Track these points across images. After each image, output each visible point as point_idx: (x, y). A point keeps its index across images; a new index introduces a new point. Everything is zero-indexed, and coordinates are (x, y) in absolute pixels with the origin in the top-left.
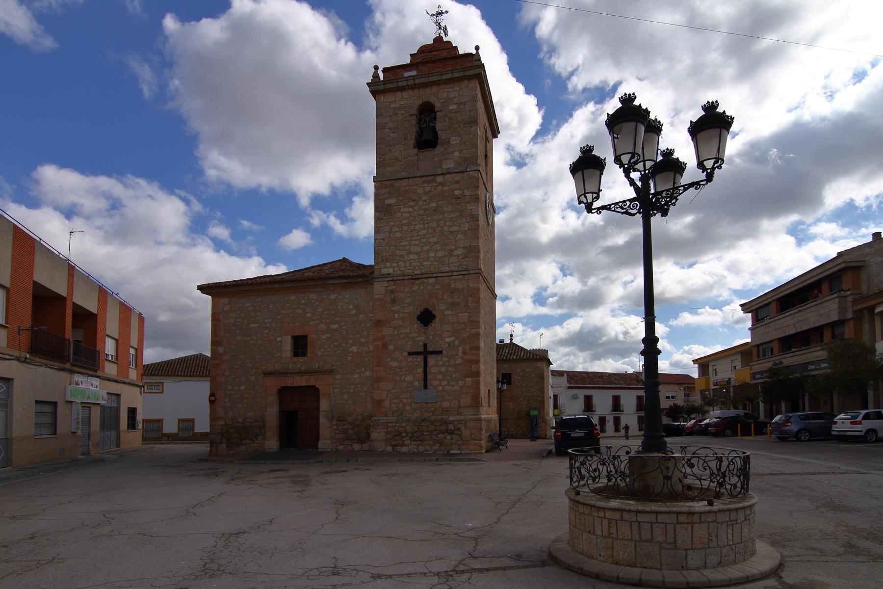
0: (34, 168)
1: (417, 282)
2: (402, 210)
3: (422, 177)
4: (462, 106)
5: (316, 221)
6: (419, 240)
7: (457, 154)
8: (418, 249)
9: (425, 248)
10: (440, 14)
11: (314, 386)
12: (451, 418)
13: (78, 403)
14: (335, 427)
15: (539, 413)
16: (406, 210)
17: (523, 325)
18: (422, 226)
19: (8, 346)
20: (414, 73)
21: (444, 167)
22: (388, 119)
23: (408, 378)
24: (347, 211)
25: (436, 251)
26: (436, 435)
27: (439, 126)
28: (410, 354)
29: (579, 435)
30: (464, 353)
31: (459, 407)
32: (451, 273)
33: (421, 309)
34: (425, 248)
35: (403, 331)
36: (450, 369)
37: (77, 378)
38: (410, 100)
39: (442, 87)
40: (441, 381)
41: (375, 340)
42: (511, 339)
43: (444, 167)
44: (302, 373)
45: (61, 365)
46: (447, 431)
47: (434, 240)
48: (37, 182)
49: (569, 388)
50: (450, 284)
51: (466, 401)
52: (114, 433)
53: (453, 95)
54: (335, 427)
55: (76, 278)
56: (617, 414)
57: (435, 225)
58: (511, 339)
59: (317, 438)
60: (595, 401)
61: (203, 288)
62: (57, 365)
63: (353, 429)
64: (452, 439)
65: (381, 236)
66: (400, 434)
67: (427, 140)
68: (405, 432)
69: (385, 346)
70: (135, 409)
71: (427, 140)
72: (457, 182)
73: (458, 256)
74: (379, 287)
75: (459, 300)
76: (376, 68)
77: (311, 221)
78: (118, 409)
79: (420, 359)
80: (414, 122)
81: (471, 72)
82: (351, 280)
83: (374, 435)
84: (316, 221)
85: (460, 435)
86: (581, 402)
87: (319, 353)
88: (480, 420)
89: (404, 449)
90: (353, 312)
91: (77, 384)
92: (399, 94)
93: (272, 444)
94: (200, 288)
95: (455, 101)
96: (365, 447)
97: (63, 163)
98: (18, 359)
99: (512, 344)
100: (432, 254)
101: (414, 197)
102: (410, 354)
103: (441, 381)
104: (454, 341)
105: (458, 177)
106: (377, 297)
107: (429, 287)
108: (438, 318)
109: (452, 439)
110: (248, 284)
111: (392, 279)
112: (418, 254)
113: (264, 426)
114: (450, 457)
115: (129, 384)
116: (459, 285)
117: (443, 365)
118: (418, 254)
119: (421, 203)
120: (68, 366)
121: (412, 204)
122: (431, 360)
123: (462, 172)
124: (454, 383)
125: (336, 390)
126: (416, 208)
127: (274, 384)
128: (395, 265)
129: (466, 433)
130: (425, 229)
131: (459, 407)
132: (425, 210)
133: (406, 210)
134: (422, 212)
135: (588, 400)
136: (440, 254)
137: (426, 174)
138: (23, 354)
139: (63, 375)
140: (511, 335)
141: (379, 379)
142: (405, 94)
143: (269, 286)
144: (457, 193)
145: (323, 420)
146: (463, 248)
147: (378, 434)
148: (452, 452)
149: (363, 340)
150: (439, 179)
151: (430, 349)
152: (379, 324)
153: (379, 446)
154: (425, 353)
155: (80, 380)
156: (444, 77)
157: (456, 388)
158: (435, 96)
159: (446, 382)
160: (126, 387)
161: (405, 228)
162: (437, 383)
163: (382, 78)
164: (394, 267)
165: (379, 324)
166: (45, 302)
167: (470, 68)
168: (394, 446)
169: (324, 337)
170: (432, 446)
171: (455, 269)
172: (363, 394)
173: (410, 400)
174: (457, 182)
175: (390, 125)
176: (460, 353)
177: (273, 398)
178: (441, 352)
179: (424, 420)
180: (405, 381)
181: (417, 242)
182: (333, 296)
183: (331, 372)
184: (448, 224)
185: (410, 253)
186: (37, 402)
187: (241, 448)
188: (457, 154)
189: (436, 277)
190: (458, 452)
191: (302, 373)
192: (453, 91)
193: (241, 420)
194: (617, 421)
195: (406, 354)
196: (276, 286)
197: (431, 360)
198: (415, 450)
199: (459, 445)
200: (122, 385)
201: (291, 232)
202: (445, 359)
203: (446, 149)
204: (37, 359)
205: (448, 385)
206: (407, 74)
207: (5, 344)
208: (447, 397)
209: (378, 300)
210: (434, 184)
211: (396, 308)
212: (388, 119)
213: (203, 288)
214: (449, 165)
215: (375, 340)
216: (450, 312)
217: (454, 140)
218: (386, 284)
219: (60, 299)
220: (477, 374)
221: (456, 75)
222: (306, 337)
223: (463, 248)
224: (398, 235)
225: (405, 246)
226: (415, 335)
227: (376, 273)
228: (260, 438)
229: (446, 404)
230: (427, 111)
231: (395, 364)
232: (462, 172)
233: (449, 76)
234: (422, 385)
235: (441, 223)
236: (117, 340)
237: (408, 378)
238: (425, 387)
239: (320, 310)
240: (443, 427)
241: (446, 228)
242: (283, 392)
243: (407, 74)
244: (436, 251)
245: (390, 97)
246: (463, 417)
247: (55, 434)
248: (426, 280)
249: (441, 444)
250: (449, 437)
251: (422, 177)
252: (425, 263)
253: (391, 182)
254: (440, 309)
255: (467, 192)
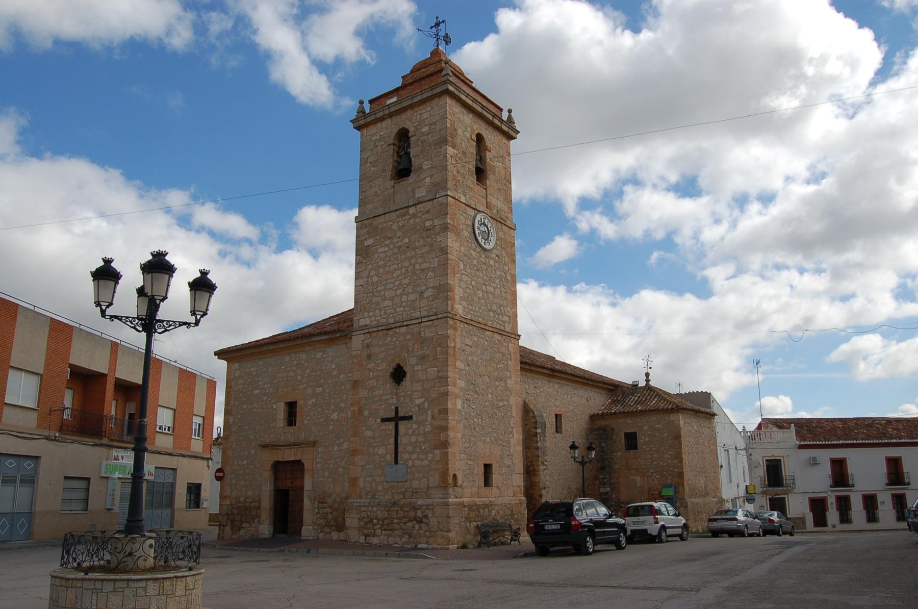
0: (295, 213)
1: (390, 332)
2: (380, 250)
3: (396, 210)
4: (433, 127)
5: (583, 226)
6: (393, 283)
7: (428, 180)
8: (392, 294)
9: (399, 292)
10: (438, 25)
11: (300, 461)
12: (419, 502)
13: (114, 479)
14: (317, 511)
15: (676, 492)
16: (382, 250)
17: (885, 336)
18: (395, 266)
19: (37, 427)
20: (395, 99)
21: (417, 196)
22: (369, 153)
23: (381, 451)
24: (617, 204)
25: (408, 294)
26: (405, 523)
27: (413, 152)
28: (383, 420)
29: (554, 527)
30: (433, 417)
31: (428, 488)
32: (420, 321)
33: (394, 365)
34: (399, 292)
35: (377, 392)
36: (420, 439)
37: (115, 452)
38: (387, 130)
39: (416, 109)
40: (410, 453)
41: (352, 405)
42: (648, 381)
43: (417, 196)
44: (290, 445)
45: (97, 441)
46: (415, 519)
47: (407, 281)
48: (296, 225)
49: (801, 447)
50: (419, 333)
51: (435, 480)
52: (167, 512)
53: (425, 116)
54: (317, 511)
55: (120, 353)
56: (898, 490)
57: (407, 264)
58: (648, 381)
59: (301, 524)
60: (906, 467)
61: (220, 354)
62: (91, 441)
63: (332, 513)
64: (420, 529)
65: (361, 282)
66: (371, 521)
67: (403, 171)
68: (376, 518)
69: (361, 412)
70: (200, 485)
71: (403, 171)
72: (428, 212)
73: (428, 298)
74: (357, 341)
75: (429, 352)
76: (361, 102)
77: (578, 225)
78: (173, 485)
79: (391, 426)
80: (391, 152)
81: (438, 90)
82: (331, 336)
83: (348, 522)
84: (583, 226)
85: (427, 524)
86: (826, 470)
87: (306, 422)
88: (447, 504)
89: (375, 541)
90: (335, 372)
91: (116, 459)
92: (379, 124)
93: (265, 529)
94: (216, 354)
95: (427, 122)
96: (342, 536)
97: (318, 202)
98: (47, 438)
99: (648, 388)
100: (404, 298)
101: (389, 235)
102: (383, 420)
103: (410, 453)
104: (424, 402)
105: (428, 206)
106: (354, 353)
107: (401, 338)
108: (408, 375)
109: (420, 529)
110: (251, 347)
111: (369, 331)
112: (392, 299)
113: (259, 507)
114: (410, 551)
115: (190, 456)
116: (428, 334)
117: (413, 434)
118: (392, 299)
119: (395, 240)
120: (105, 441)
121: (388, 242)
122: (402, 426)
123: (432, 200)
124: (423, 457)
125: (319, 465)
126: (391, 246)
127: (269, 458)
128: (371, 314)
129: (433, 521)
130: (398, 269)
131: (428, 488)
132: (400, 247)
133: (382, 250)
134: (396, 250)
135: (839, 466)
136: (412, 297)
137: (400, 207)
138: (52, 433)
139: (104, 450)
140: (647, 375)
141: (354, 452)
142: (384, 124)
143: (266, 348)
144: (428, 224)
145: (306, 502)
146: (433, 288)
147: (352, 521)
148: (420, 546)
149: (342, 405)
150: (412, 210)
151: (401, 414)
152: (356, 385)
153: (354, 535)
154: (397, 419)
155: (120, 455)
156: (415, 100)
157: (426, 462)
158: (407, 121)
159: (414, 456)
160: (186, 460)
161: (381, 270)
162: (407, 456)
163: (367, 111)
164: (370, 317)
165: (356, 385)
166: (85, 381)
167: (437, 86)
168: (367, 536)
169: (310, 403)
170: (401, 537)
171: (426, 313)
172: (341, 470)
173: (382, 479)
174: (428, 212)
175: (371, 159)
176: (429, 419)
177: (268, 475)
178: (411, 418)
179: (394, 504)
180: (377, 454)
181: (391, 286)
182: (319, 355)
183: (314, 444)
184: (419, 261)
185: (385, 299)
186: (66, 478)
187: (242, 532)
188: (428, 180)
189: (407, 325)
190: (425, 546)
191: (290, 445)
192: (425, 113)
193: (242, 499)
194: (899, 501)
195: (379, 421)
196: (272, 347)
197: (402, 426)
198: (385, 542)
199: (427, 537)
200: (180, 458)
201: (553, 240)
202: (415, 426)
203: (418, 176)
204: (69, 437)
205: (418, 459)
206: (389, 102)
207: (34, 425)
208: (417, 475)
209: (356, 357)
210: (407, 217)
211: (371, 366)
212: (369, 153)
213: (220, 354)
214: (421, 193)
215: (352, 405)
216: (419, 368)
217: (426, 165)
218: (362, 337)
219: (102, 377)
220: (445, 445)
221: (425, 96)
222: (296, 402)
223: (433, 288)
224: (375, 279)
225: (380, 291)
226: (384, 397)
227: (355, 325)
228: (256, 520)
229: (415, 484)
230: (403, 136)
231: (369, 433)
232: (432, 200)
233: (419, 98)
234: (390, 458)
235: (413, 261)
236: (175, 410)
237: (381, 451)
238: (396, 462)
239: (308, 371)
240: (412, 514)
241: (417, 267)
242: (278, 466)
243: (389, 102)
244: (408, 294)
245: (372, 130)
246: (430, 501)
247: (86, 510)
248: (398, 330)
249: (410, 536)
250: (417, 526)
251: (396, 210)
252: (398, 310)
253: (369, 221)
254: (411, 365)
255: (437, 222)
